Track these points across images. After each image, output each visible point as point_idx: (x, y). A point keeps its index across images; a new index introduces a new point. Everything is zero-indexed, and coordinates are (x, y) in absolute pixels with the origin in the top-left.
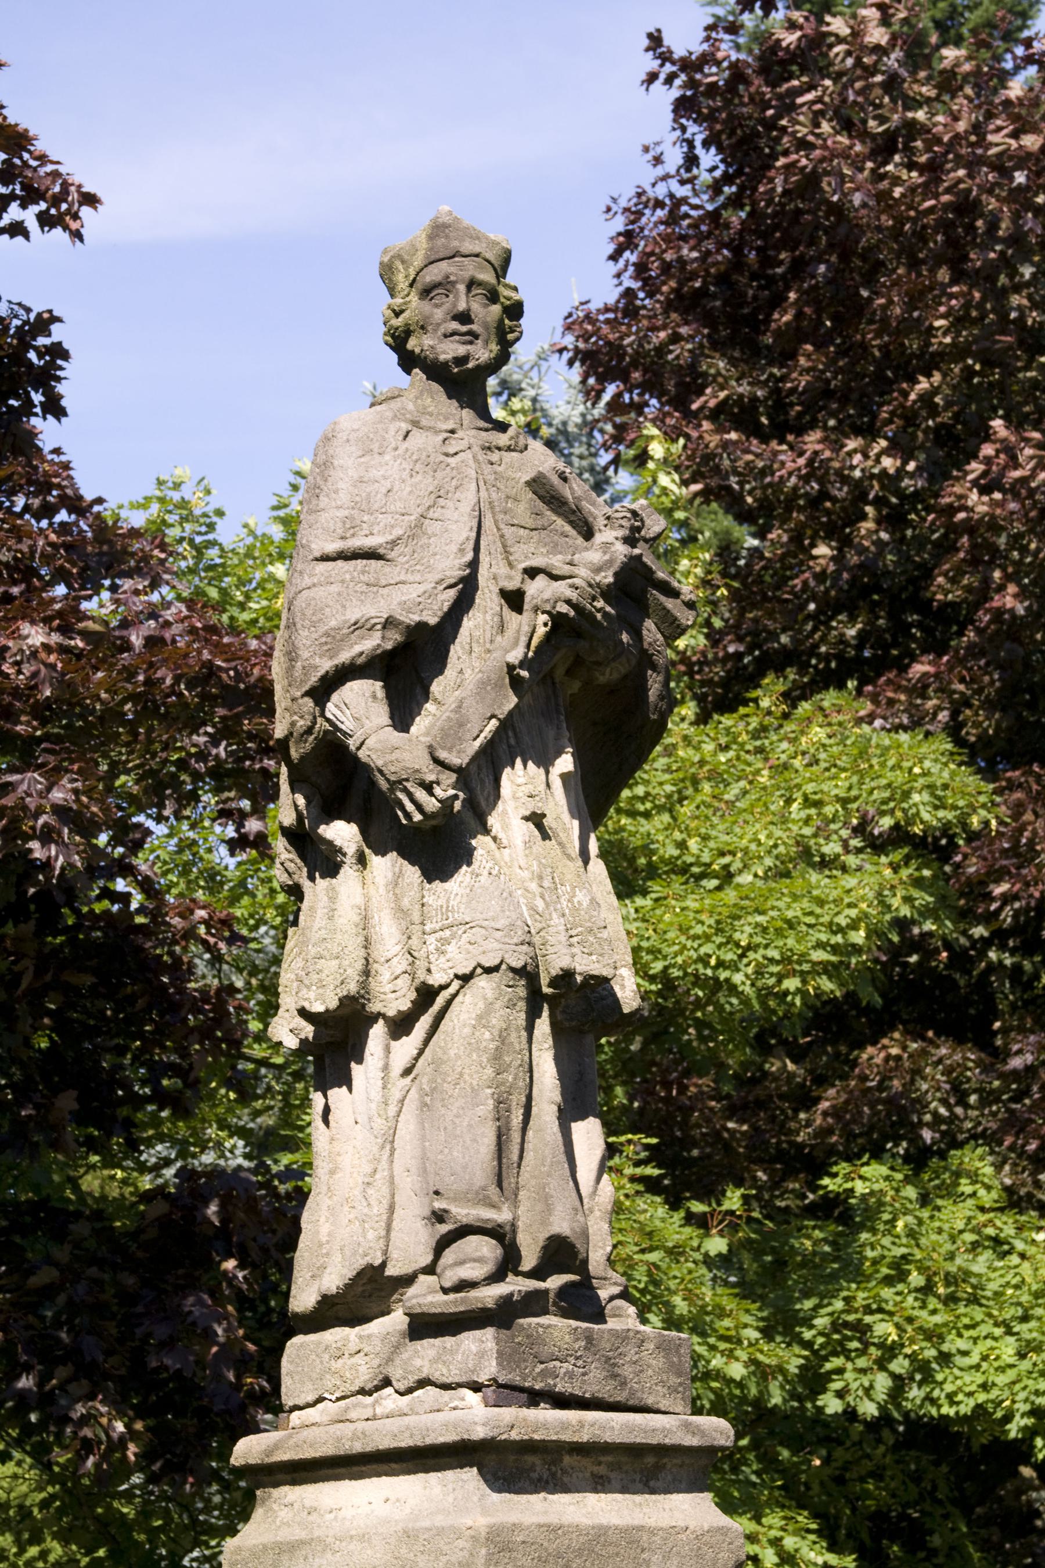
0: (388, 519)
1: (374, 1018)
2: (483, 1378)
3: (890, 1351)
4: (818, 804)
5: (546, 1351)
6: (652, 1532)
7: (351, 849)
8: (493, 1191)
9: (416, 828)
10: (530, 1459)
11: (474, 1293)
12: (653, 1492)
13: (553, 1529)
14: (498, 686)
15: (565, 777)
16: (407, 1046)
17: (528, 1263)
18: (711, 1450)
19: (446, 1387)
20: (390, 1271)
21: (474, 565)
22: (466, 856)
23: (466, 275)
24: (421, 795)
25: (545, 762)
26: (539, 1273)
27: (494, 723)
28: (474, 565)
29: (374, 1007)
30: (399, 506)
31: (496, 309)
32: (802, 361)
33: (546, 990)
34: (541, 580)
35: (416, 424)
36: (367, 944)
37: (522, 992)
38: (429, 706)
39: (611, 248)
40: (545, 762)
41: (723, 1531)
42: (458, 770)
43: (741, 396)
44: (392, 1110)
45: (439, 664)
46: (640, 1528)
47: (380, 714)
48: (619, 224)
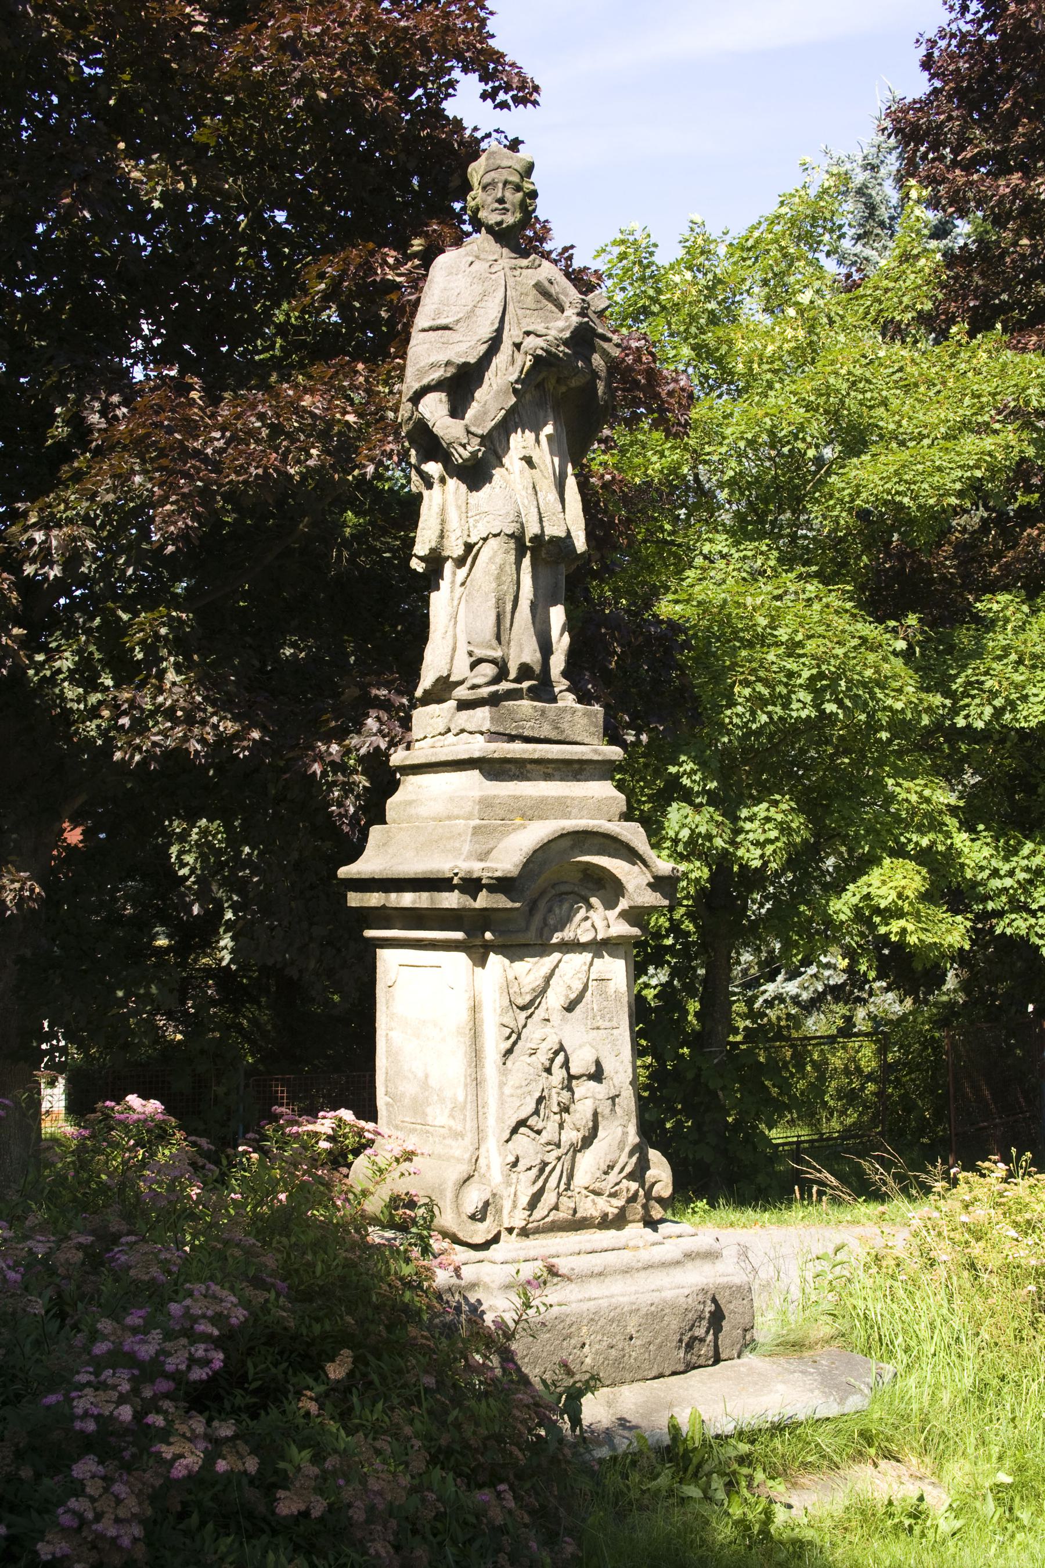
0: (457, 309)
1: (447, 558)
2: (484, 729)
3: (994, 694)
4: (979, 397)
5: (518, 717)
6: (573, 799)
7: (436, 476)
8: (494, 642)
9: (459, 465)
10: (508, 766)
11: (480, 690)
12: (578, 780)
13: (516, 798)
14: (506, 393)
15: (549, 437)
16: (463, 572)
17: (513, 675)
18: (611, 762)
19: (471, 733)
20: (452, 679)
21: (500, 331)
22: (489, 478)
23: (503, 178)
24: (461, 450)
25: (536, 430)
26: (518, 680)
27: (503, 412)
28: (500, 331)
29: (445, 554)
30: (463, 302)
31: (520, 195)
32: (1020, 129)
33: (528, 544)
34: (532, 336)
35: (477, 257)
36: (443, 522)
37: (513, 546)
38: (474, 404)
40: (536, 430)
41: (615, 798)
42: (482, 437)
43: (988, 150)
44: (456, 603)
45: (480, 383)
46: (566, 797)
47: (444, 409)
48: (922, 51)
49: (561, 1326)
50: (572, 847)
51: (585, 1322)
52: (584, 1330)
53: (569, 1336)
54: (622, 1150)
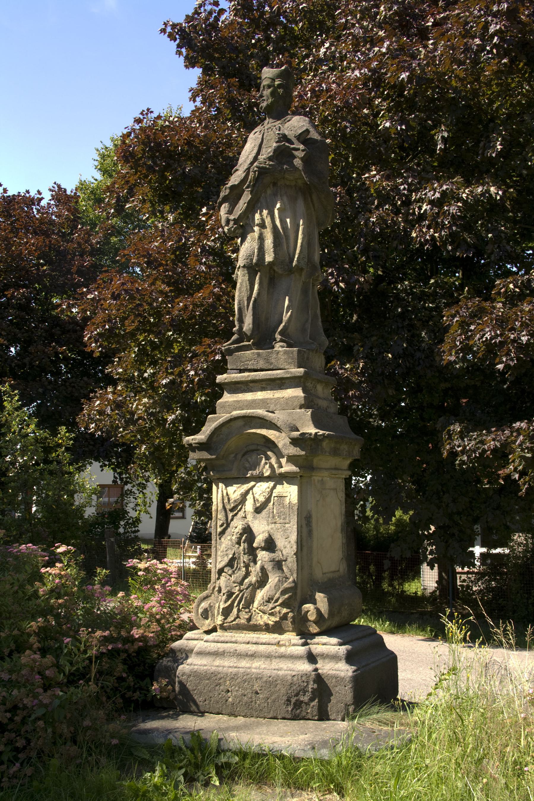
5: (243, 360)
10: (239, 386)
12: (282, 389)
37: (246, 272)
39: (101, 469)
46: (267, 399)
49: (214, 678)
50: (244, 425)
51: (228, 679)
52: (228, 683)
53: (220, 684)
54: (278, 590)
